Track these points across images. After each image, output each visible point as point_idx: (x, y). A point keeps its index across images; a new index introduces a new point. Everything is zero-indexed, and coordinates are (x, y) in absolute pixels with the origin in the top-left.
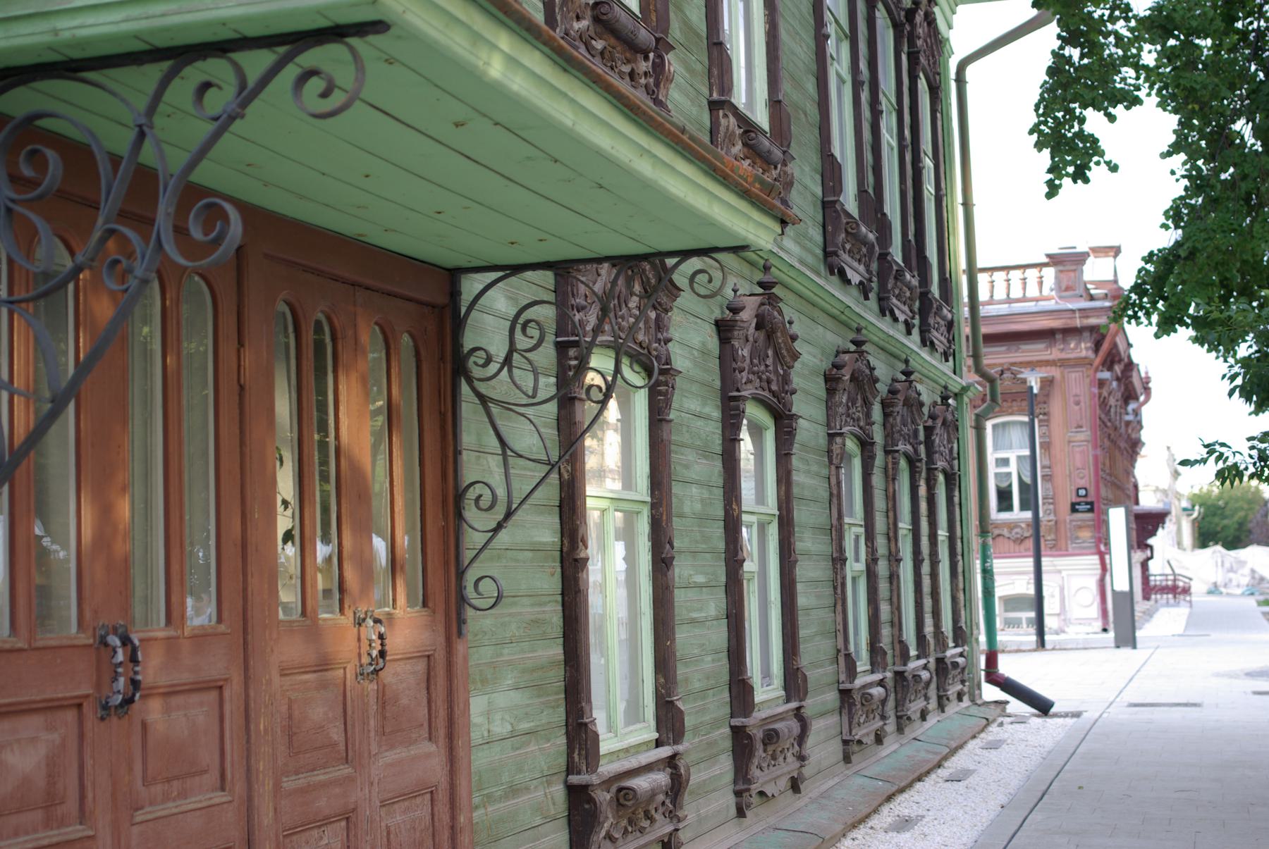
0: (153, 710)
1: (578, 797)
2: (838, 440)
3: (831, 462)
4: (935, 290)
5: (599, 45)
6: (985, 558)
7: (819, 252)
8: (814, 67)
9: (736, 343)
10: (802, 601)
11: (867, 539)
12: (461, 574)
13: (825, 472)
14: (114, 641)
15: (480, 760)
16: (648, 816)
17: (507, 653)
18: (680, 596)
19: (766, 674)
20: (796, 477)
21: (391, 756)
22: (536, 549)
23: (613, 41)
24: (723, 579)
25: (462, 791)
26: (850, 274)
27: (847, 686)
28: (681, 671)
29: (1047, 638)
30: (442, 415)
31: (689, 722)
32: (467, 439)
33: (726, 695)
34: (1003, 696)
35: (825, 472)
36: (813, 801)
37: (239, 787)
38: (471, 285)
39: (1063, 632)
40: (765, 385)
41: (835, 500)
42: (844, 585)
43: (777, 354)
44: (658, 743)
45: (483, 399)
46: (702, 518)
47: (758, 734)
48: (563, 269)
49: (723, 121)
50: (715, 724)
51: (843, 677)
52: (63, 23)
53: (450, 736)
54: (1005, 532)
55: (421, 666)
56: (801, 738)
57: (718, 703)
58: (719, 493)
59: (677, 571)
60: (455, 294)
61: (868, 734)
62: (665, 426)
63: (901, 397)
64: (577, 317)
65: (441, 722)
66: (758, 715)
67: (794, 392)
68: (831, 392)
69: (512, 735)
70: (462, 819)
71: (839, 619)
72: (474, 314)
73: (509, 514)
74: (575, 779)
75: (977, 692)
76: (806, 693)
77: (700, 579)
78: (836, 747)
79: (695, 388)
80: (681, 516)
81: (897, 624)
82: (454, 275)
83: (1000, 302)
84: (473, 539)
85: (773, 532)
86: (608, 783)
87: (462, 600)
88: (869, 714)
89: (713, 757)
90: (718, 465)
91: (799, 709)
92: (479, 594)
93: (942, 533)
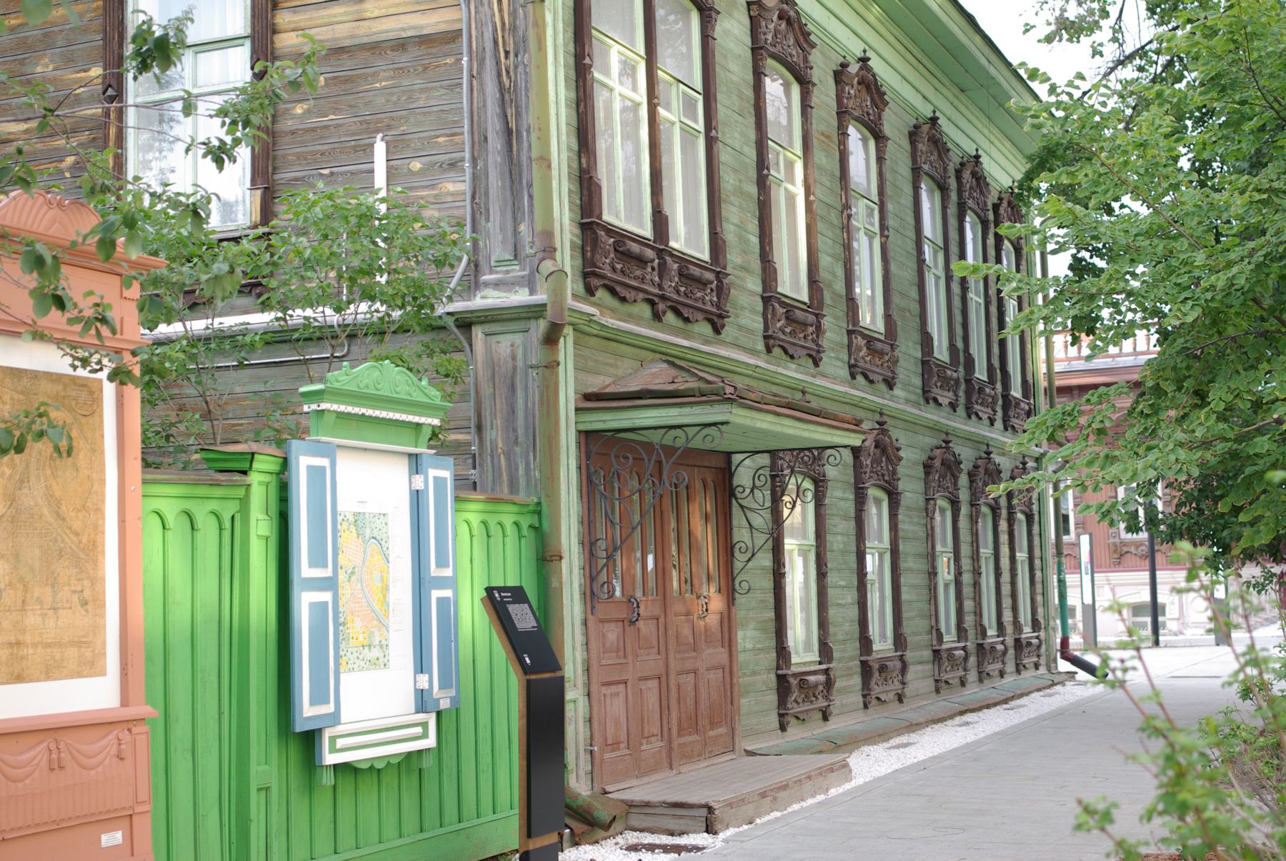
0: (641, 624)
1: (782, 680)
2: (932, 502)
3: (927, 515)
4: (1016, 393)
5: (788, 330)
6: (1060, 572)
7: (920, 391)
8: (916, 280)
9: (862, 458)
10: (905, 596)
11: (955, 561)
12: (733, 580)
13: (923, 521)
14: (633, 600)
15: (742, 658)
16: (815, 696)
17: (751, 614)
18: (831, 592)
19: (883, 636)
20: (901, 526)
21: (710, 651)
22: (763, 568)
23: (795, 325)
24: (856, 583)
25: (735, 669)
26: (941, 400)
27: (938, 648)
28: (832, 629)
29: (1161, 638)
30: (725, 514)
31: (835, 655)
32: (735, 523)
33: (858, 644)
34: (1073, 668)
35: (923, 521)
36: (911, 709)
37: (664, 654)
38: (737, 458)
39: (1182, 633)
40: (881, 477)
41: (930, 538)
42: (935, 588)
43: (888, 458)
44: (820, 663)
45: (742, 507)
46: (844, 552)
47: (876, 666)
48: (773, 453)
49: (855, 341)
50: (851, 658)
51: (935, 643)
52: (636, 421)
53: (730, 646)
54: (1133, 549)
55: (718, 617)
56: (904, 670)
57: (854, 647)
58: (853, 538)
59: (829, 579)
60: (729, 462)
61: (953, 678)
62: (823, 508)
63: (982, 470)
64: (763, 37)
65: (665, 734)
66: (875, 656)
67: (899, 479)
68: (927, 474)
69: (754, 649)
70: (735, 680)
71: (933, 608)
72: (739, 468)
73: (753, 555)
74: (780, 672)
75: (1053, 665)
76: (906, 647)
77: (843, 583)
78: (930, 683)
79: (839, 485)
80: (832, 551)
81: (978, 613)
82: (729, 455)
83: (1128, 355)
84: (738, 565)
85: (887, 557)
86: (795, 675)
87: (734, 590)
88: (954, 667)
89: (850, 675)
90: (853, 523)
91: (902, 656)
92: (741, 587)
93: (1021, 556)
